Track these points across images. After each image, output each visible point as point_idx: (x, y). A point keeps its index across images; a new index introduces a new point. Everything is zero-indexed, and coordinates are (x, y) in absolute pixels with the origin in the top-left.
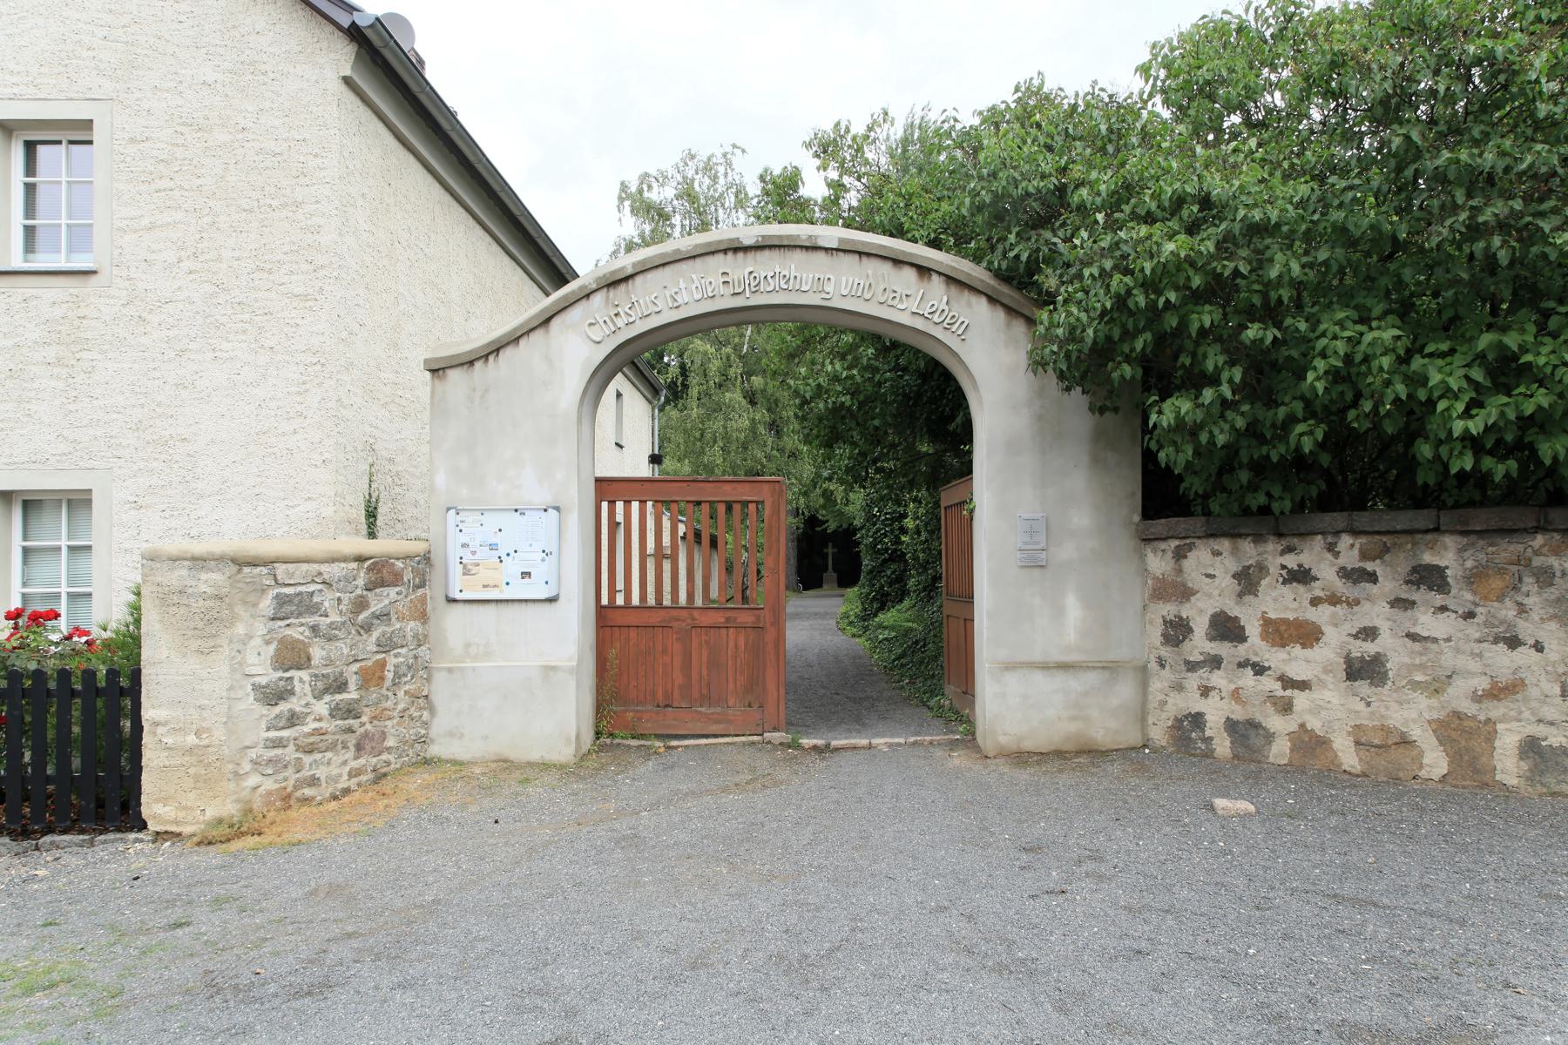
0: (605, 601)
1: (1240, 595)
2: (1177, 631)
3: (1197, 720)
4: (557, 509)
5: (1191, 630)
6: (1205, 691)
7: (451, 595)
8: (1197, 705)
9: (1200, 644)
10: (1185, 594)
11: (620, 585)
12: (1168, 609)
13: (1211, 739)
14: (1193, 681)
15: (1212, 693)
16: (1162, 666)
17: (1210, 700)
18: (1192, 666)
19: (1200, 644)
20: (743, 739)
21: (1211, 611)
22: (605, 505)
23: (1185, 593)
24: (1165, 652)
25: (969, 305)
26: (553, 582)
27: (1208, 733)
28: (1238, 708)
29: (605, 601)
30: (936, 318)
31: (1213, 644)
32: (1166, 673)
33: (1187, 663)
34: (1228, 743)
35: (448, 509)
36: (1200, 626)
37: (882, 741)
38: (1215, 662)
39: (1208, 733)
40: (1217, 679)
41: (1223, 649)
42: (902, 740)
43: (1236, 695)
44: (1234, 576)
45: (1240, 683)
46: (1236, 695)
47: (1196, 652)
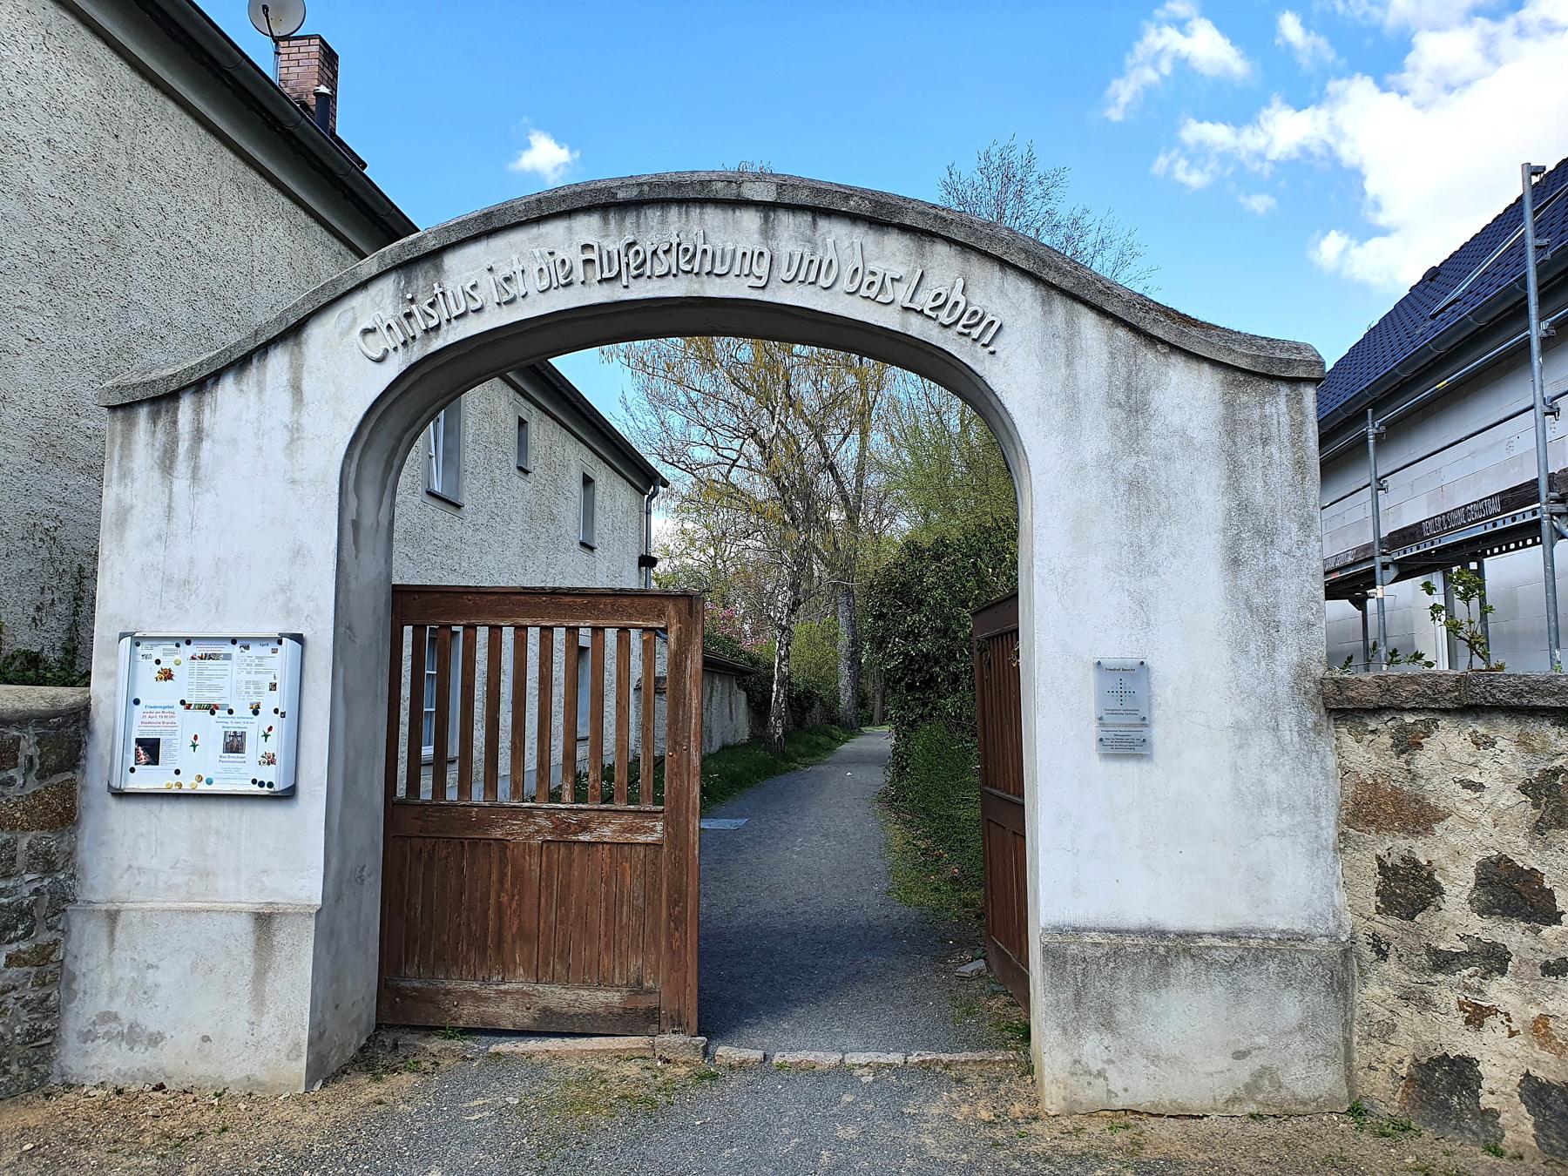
0: (401, 790)
1: (1539, 828)
2: (1408, 889)
3: (1463, 1072)
4: (298, 638)
5: (1437, 890)
6: (1477, 1016)
7: (115, 784)
8: (1463, 1042)
9: (1457, 918)
10: (1421, 816)
11: (584, 730)
12: (1396, 845)
13: (1495, 1114)
14: (1448, 991)
15: (1490, 1021)
16: (1383, 955)
17: (1487, 1035)
18: (1443, 962)
19: (1457, 918)
20: (595, 1043)
21: (1476, 857)
22: (408, 630)
23: (1421, 816)
24: (1387, 926)
25: (1002, 292)
26: (147, 779)
27: (1486, 1101)
28: (1545, 1055)
29: (401, 790)
30: (943, 317)
31: (1487, 923)
32: (1391, 967)
33: (1433, 952)
34: (1528, 1127)
35: (123, 636)
36: (1459, 882)
37: (862, 1058)
38: (1495, 960)
39: (1486, 1101)
40: (1499, 992)
41: (1513, 935)
42: (897, 1058)
43: (1541, 1029)
44: (1523, 789)
45: (1551, 1006)
46: (1541, 1029)
47: (1451, 933)
